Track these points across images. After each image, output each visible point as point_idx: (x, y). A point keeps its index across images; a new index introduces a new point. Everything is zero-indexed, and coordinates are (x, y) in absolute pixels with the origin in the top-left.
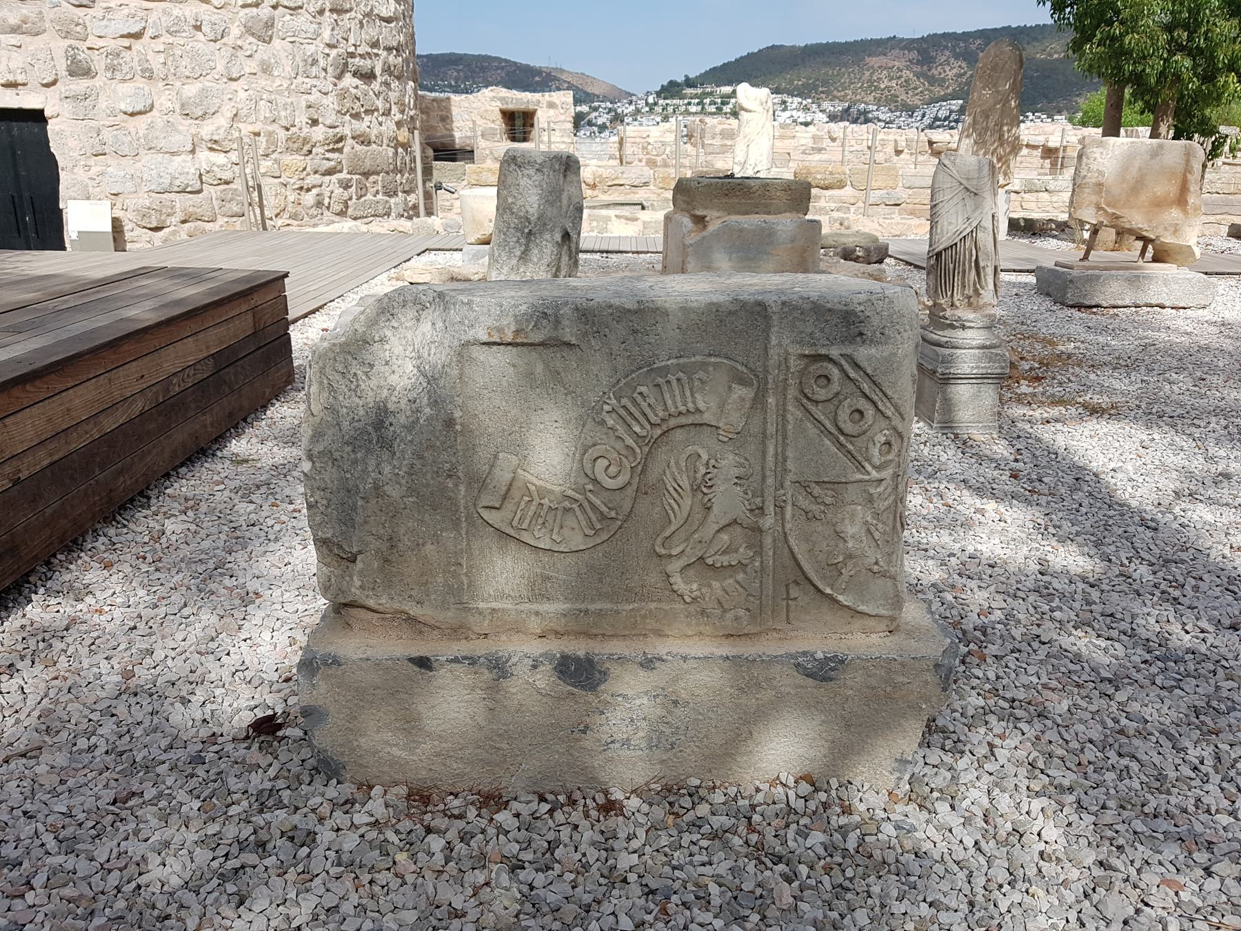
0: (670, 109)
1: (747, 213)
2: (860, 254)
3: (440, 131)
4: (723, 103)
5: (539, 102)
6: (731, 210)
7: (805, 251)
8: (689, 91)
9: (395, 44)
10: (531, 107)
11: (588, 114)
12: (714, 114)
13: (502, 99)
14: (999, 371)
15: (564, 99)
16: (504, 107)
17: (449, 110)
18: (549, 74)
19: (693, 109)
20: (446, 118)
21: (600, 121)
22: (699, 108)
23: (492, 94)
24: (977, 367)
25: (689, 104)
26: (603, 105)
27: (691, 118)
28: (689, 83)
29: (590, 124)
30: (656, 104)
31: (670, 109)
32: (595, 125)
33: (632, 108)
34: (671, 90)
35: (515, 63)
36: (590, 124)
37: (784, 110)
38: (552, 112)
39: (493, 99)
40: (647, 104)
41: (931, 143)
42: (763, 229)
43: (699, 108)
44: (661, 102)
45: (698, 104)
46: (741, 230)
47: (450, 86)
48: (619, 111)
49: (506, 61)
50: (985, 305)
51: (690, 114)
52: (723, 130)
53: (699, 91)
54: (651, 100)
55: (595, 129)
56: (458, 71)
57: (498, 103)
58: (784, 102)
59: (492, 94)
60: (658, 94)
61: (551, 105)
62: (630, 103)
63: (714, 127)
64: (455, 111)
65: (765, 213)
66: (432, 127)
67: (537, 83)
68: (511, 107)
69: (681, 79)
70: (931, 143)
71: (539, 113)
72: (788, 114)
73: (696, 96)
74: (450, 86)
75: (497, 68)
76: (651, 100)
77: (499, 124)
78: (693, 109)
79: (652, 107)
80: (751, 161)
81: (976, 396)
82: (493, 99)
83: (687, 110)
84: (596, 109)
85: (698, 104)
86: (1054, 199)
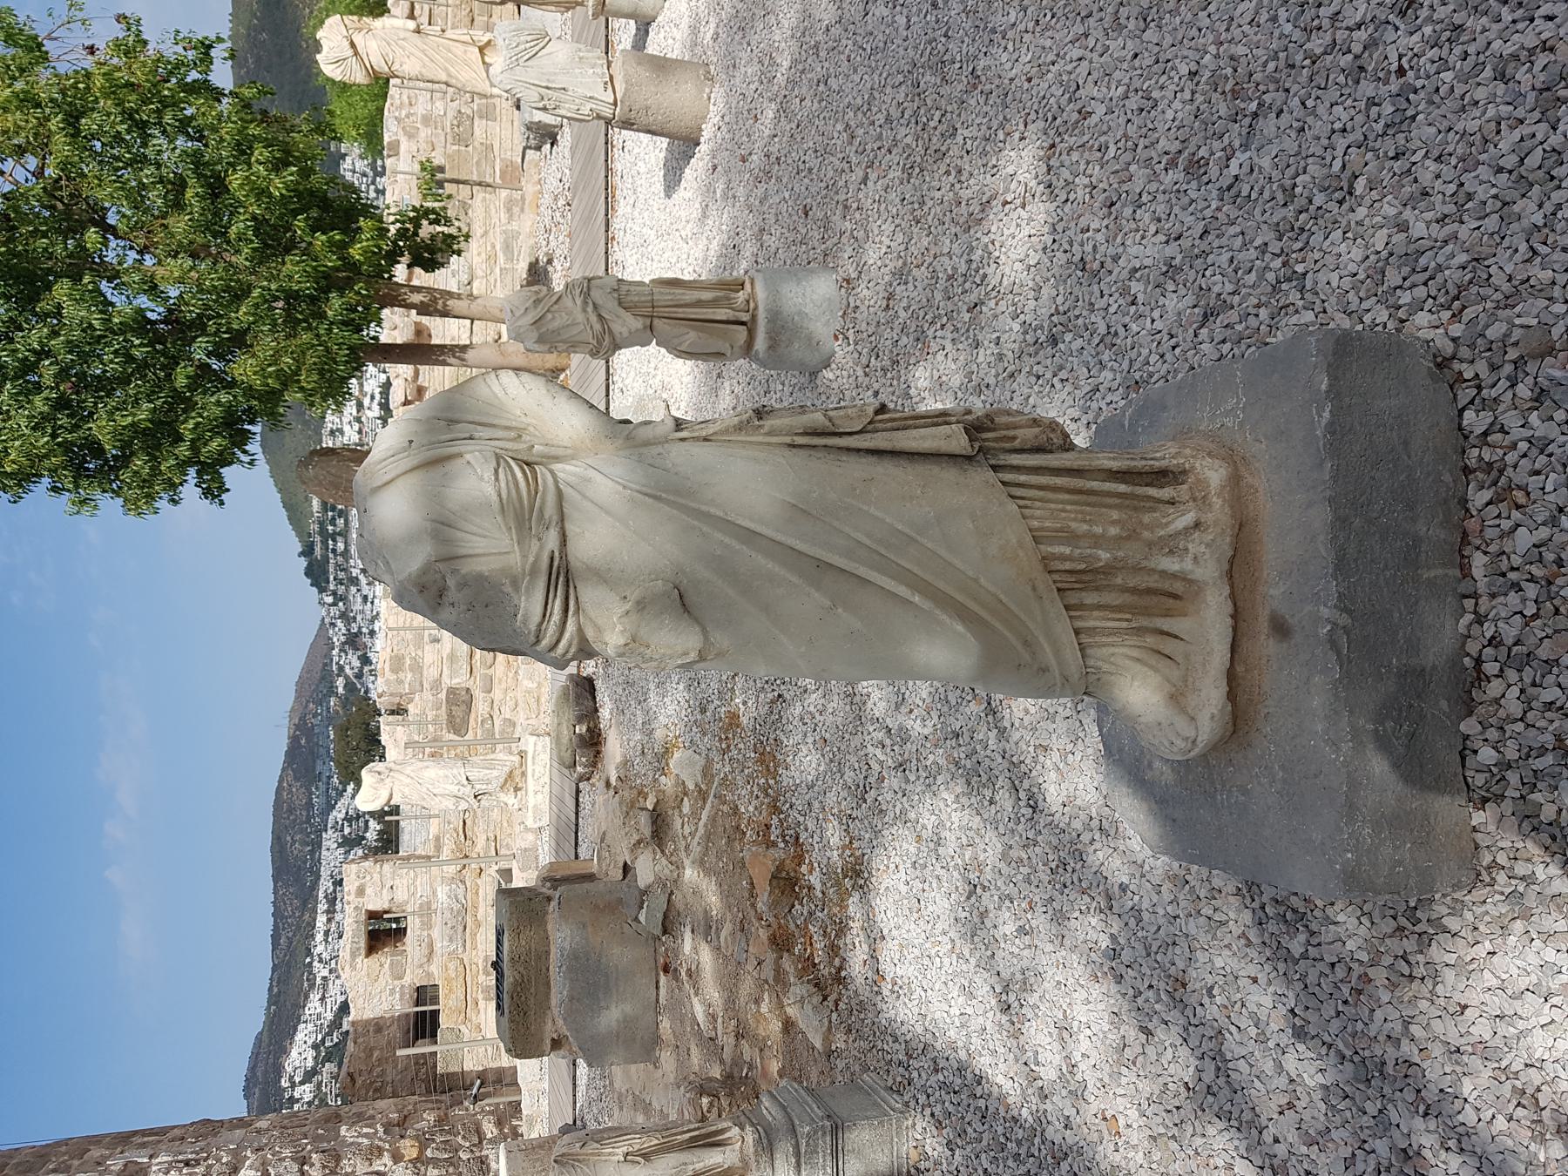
0: (341, 575)
1: (548, 984)
2: (584, 729)
3: (395, 1032)
4: (333, 509)
5: (356, 908)
6: (544, 1005)
7: (597, 906)
8: (318, 550)
9: (296, 1167)
10: (363, 917)
11: (347, 677)
12: (346, 521)
13: (354, 955)
14: (828, 1138)
15: (353, 876)
16: (363, 952)
17: (368, 1022)
18: (297, 727)
19: (341, 546)
20: (378, 1026)
21: (356, 663)
22: (339, 539)
23: (347, 968)
24: (824, 1167)
25: (334, 551)
26: (335, 659)
27: (353, 549)
28: (308, 551)
29: (359, 676)
30: (334, 593)
31: (341, 575)
32: (361, 669)
33: (339, 623)
34: (317, 574)
35: (283, 770)
36: (359, 676)
37: (341, 432)
38: (369, 891)
39: (353, 968)
40: (334, 604)
41: (406, 403)
42: (570, 969)
43: (339, 539)
44: (332, 587)
45: (334, 540)
46: (571, 999)
47: (312, 852)
48: (343, 639)
49: (280, 782)
50: (743, 1160)
51: (347, 550)
52: (392, 670)
53: (318, 539)
54: (330, 600)
55: (366, 669)
56: (294, 842)
57: (358, 960)
58: (332, 432)
59: (347, 968)
60: (322, 590)
61: (361, 892)
62: (333, 625)
63: (388, 682)
64: (369, 1015)
65: (547, 959)
66: (389, 1043)
67: (308, 742)
68: (363, 944)
69: (303, 562)
70: (406, 403)
71: (371, 907)
72: (347, 428)
73: (325, 543)
74: (312, 852)
75: (290, 792)
76: (330, 600)
77: (385, 958)
78: (341, 546)
79: (338, 598)
80: (454, 789)
81: (858, 1153)
82: (353, 968)
83: (342, 554)
84: (341, 668)
85: (334, 540)
86: (479, 273)
